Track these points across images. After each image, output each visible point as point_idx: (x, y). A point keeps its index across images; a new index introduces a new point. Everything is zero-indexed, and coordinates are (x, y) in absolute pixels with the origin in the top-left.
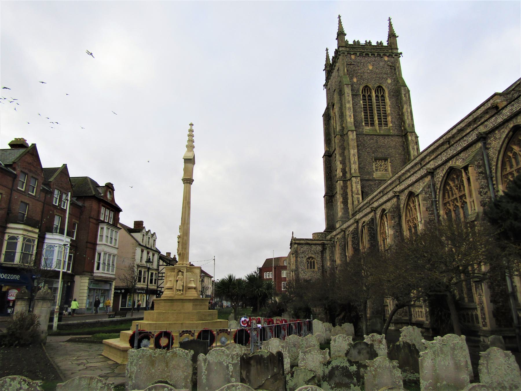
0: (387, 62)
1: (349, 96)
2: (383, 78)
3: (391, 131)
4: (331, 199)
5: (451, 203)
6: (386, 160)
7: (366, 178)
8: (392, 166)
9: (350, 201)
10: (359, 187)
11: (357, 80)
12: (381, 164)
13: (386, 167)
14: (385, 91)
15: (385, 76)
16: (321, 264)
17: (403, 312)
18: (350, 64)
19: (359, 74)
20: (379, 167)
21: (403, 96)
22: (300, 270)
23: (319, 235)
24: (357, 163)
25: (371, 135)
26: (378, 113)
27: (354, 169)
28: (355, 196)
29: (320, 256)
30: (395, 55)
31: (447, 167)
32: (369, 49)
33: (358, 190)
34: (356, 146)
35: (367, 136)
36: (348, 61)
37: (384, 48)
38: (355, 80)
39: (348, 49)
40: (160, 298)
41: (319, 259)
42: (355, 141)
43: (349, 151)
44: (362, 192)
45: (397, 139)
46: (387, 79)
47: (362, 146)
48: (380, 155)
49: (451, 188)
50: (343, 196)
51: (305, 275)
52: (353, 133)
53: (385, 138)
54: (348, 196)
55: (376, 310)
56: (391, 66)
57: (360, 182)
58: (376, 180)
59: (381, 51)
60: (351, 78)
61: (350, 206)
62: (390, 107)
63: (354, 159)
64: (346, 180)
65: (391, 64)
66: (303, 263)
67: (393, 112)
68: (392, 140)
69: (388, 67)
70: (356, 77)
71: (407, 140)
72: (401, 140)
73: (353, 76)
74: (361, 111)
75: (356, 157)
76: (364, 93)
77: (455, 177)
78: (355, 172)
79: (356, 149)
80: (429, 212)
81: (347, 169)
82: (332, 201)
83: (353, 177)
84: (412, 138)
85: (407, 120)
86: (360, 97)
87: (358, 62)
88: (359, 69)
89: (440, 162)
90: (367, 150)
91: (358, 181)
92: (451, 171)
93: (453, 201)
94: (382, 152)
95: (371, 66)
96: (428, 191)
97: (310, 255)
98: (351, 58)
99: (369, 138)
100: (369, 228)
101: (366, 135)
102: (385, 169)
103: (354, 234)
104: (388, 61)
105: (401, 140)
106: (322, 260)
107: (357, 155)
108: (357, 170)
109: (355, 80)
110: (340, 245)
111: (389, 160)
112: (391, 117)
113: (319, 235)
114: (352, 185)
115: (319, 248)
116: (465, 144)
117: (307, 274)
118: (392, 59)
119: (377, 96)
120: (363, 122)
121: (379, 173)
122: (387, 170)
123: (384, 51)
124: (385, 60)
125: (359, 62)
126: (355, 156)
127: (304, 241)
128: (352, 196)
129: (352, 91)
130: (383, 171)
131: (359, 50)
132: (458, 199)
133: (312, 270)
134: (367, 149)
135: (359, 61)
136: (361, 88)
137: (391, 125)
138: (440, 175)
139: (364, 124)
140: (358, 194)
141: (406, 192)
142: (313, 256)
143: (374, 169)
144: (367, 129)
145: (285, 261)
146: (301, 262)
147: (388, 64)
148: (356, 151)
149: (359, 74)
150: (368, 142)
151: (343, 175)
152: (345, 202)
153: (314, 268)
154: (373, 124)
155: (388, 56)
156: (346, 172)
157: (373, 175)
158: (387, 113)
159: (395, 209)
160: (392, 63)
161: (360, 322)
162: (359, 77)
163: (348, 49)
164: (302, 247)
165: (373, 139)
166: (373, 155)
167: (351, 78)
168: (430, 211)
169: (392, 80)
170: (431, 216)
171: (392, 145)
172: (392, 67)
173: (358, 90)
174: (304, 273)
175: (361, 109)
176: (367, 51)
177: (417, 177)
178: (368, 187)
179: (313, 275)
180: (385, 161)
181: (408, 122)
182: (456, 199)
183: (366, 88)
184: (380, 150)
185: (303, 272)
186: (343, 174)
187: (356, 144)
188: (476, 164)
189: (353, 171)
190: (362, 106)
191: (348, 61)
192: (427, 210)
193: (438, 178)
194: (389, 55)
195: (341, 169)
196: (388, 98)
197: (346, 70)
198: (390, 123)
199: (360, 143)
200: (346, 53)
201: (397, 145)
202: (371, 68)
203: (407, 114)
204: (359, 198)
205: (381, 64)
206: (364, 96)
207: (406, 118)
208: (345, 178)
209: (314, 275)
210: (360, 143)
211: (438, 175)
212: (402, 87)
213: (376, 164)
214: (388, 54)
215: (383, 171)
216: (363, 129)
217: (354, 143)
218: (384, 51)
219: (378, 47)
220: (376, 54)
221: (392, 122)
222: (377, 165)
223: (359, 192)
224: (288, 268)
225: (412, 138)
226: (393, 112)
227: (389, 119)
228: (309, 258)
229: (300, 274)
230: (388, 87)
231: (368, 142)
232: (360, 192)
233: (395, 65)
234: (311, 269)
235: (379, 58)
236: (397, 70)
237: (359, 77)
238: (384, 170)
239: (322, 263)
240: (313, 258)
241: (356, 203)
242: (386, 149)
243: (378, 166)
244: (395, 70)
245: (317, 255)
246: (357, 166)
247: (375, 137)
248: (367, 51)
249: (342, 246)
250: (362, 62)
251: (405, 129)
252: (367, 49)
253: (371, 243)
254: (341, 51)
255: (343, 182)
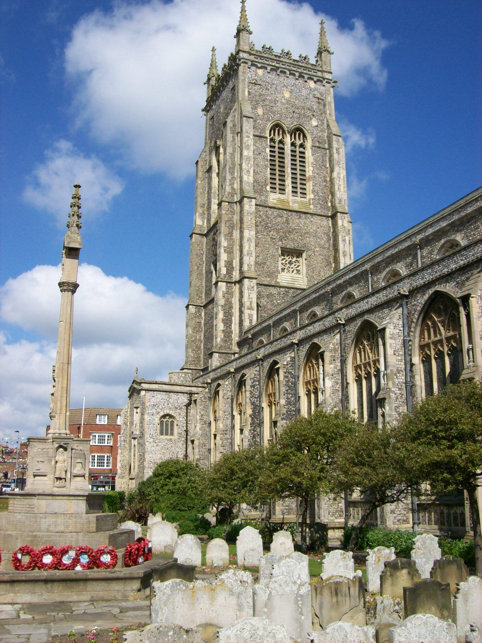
0: (314, 91)
1: (248, 137)
2: (305, 116)
3: (312, 207)
4: (199, 311)
5: (432, 347)
6: (299, 253)
7: (266, 283)
8: (308, 266)
9: (235, 319)
10: (254, 296)
11: (264, 113)
12: (290, 261)
13: (298, 266)
14: (306, 137)
15: (309, 113)
16: (185, 428)
17: (336, 512)
18: (255, 84)
19: (267, 103)
20: (288, 265)
21: (335, 151)
22: (147, 436)
23: (181, 376)
24: (254, 255)
25: (279, 209)
26: (292, 173)
27: (248, 265)
28: (246, 312)
29: (183, 413)
30: (327, 82)
31: (431, 291)
32: (287, 64)
33: (251, 302)
34: (254, 226)
35: (272, 210)
36: (252, 77)
37: (309, 66)
38: (260, 111)
39: (252, 58)
40: (97, 517)
41: (181, 419)
42: (253, 215)
43: (241, 232)
44: (258, 305)
45: (319, 222)
46: (311, 119)
47: (263, 226)
48: (290, 245)
49: (434, 323)
50: (224, 309)
51: (155, 445)
52: (251, 201)
53: (300, 217)
54: (233, 310)
55: (287, 508)
56: (319, 99)
57: (255, 288)
58: (281, 287)
59: (305, 72)
60: (255, 108)
61: (235, 328)
62: (313, 167)
63: (249, 248)
64: (232, 283)
65: (318, 95)
66: (154, 424)
67: (316, 175)
68: (312, 221)
69: (314, 99)
70: (262, 106)
71: (335, 225)
72: (325, 223)
73: (258, 104)
74: (266, 166)
75: (253, 245)
76: (272, 135)
77: (442, 307)
78: (249, 270)
79: (254, 230)
80: (397, 358)
81: (236, 263)
82: (201, 315)
83: (246, 278)
84: (343, 222)
85: (338, 192)
86: (266, 141)
87: (267, 82)
88: (268, 95)
89: (421, 282)
90: (271, 234)
91: (252, 285)
92: (436, 297)
93: (435, 343)
94: (293, 240)
95: (288, 93)
96: (398, 325)
97: (167, 411)
98: (256, 74)
99: (275, 213)
100: (285, 373)
101: (271, 207)
102: (297, 270)
103: (254, 381)
104: (315, 89)
105: (325, 223)
106: (187, 420)
107: (253, 241)
108: (253, 267)
109: (260, 111)
110: (223, 397)
111: (304, 255)
112: (313, 182)
113: (181, 376)
114: (241, 293)
115: (184, 399)
116: (462, 260)
117: (159, 444)
118: (322, 88)
119: (293, 144)
120: (267, 185)
121: (287, 274)
122: (299, 271)
123: (310, 73)
124: (310, 87)
125: (268, 83)
126: (251, 241)
127: (157, 385)
128: (241, 312)
129: (254, 128)
130: (293, 271)
131: (271, 63)
132: (444, 341)
133: (168, 437)
134: (270, 231)
135: (269, 80)
136: (269, 126)
137: (312, 196)
138: (419, 301)
139: (268, 188)
140: (251, 308)
141: (359, 322)
142: (172, 413)
143: (280, 268)
144: (273, 198)
145: (98, 416)
146: (150, 422)
147: (315, 95)
148: (253, 233)
149: (267, 103)
150: (273, 220)
151: (227, 272)
152: (227, 320)
153: (172, 434)
154: (282, 191)
155: (315, 82)
156: (233, 268)
157: (277, 278)
158: (307, 176)
159: (337, 347)
160: (321, 94)
161: (343, 540)
162: (268, 108)
163: (252, 58)
164: (153, 397)
165: (282, 217)
166: (280, 243)
167: (255, 108)
168: (398, 356)
169: (318, 122)
170: (400, 363)
171: (311, 231)
172: (320, 101)
173: (263, 130)
174: (154, 441)
175: (266, 163)
176: (284, 66)
177: (380, 298)
178: (268, 298)
179: (170, 446)
180: (298, 257)
181: (338, 196)
182: (440, 341)
183: (277, 127)
184: (292, 236)
185: (152, 440)
186: (227, 270)
187: (254, 222)
188: (479, 294)
189: (245, 268)
190: (269, 158)
191: (252, 77)
192: (395, 354)
193: (415, 305)
194: (318, 80)
195: (225, 261)
196: (310, 151)
197: (246, 93)
198: (311, 192)
199: (260, 220)
200: (250, 63)
201: (319, 230)
202: (287, 95)
203: (338, 182)
204: (252, 315)
205: (304, 92)
206: (272, 140)
207: (336, 189)
208: (231, 277)
209: (172, 447)
210: (260, 220)
211: (415, 301)
212: (334, 136)
213: (283, 260)
214: (315, 79)
215: (293, 271)
216: (267, 197)
217: (251, 219)
218: (310, 73)
219: (300, 64)
220: (297, 74)
221: (313, 191)
222: (284, 262)
223: (253, 305)
224: (122, 431)
225: (343, 222)
226: (316, 175)
227: (309, 186)
228: (164, 416)
229: (147, 443)
230: (312, 133)
231: (273, 220)
232: (254, 305)
233: (325, 98)
234: (162, 437)
235: (301, 81)
236: (327, 107)
237: (268, 108)
238: (295, 271)
239: (187, 426)
240: (171, 416)
241: (247, 324)
242: (301, 236)
243: (286, 264)
244: (325, 106)
245: (178, 411)
246: (253, 259)
247: (285, 212)
248: (284, 66)
249: (228, 398)
250: (273, 84)
251: (333, 207)
252: (284, 63)
253: (288, 398)
254: (243, 58)
255: (227, 285)
